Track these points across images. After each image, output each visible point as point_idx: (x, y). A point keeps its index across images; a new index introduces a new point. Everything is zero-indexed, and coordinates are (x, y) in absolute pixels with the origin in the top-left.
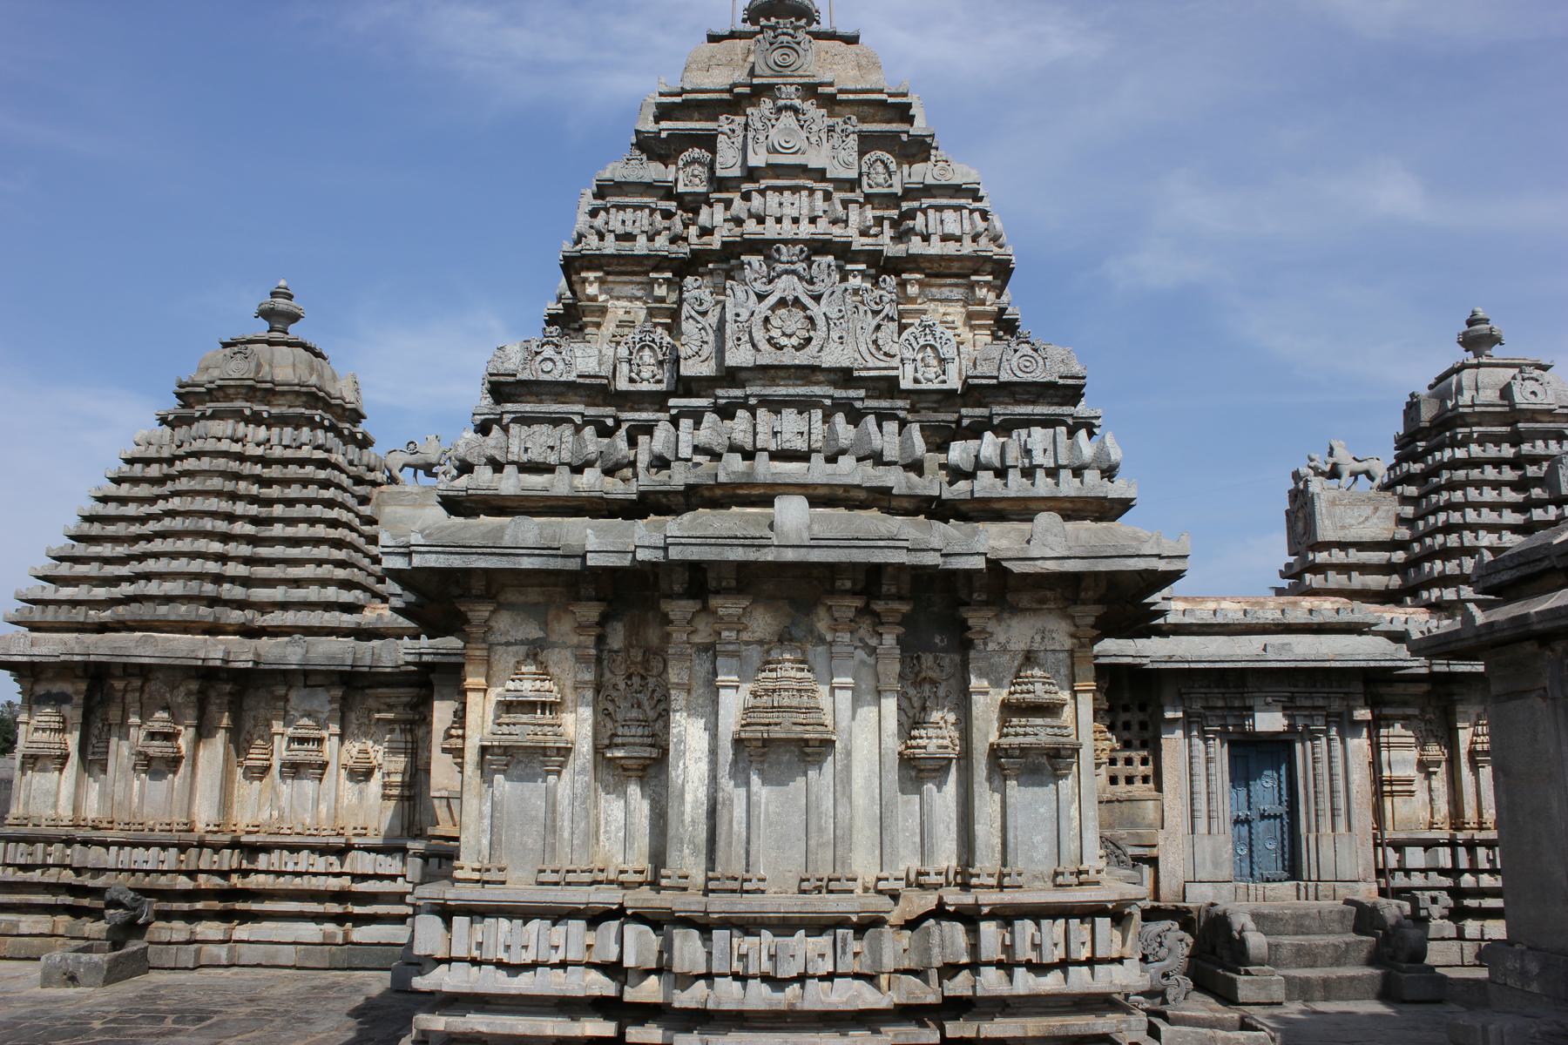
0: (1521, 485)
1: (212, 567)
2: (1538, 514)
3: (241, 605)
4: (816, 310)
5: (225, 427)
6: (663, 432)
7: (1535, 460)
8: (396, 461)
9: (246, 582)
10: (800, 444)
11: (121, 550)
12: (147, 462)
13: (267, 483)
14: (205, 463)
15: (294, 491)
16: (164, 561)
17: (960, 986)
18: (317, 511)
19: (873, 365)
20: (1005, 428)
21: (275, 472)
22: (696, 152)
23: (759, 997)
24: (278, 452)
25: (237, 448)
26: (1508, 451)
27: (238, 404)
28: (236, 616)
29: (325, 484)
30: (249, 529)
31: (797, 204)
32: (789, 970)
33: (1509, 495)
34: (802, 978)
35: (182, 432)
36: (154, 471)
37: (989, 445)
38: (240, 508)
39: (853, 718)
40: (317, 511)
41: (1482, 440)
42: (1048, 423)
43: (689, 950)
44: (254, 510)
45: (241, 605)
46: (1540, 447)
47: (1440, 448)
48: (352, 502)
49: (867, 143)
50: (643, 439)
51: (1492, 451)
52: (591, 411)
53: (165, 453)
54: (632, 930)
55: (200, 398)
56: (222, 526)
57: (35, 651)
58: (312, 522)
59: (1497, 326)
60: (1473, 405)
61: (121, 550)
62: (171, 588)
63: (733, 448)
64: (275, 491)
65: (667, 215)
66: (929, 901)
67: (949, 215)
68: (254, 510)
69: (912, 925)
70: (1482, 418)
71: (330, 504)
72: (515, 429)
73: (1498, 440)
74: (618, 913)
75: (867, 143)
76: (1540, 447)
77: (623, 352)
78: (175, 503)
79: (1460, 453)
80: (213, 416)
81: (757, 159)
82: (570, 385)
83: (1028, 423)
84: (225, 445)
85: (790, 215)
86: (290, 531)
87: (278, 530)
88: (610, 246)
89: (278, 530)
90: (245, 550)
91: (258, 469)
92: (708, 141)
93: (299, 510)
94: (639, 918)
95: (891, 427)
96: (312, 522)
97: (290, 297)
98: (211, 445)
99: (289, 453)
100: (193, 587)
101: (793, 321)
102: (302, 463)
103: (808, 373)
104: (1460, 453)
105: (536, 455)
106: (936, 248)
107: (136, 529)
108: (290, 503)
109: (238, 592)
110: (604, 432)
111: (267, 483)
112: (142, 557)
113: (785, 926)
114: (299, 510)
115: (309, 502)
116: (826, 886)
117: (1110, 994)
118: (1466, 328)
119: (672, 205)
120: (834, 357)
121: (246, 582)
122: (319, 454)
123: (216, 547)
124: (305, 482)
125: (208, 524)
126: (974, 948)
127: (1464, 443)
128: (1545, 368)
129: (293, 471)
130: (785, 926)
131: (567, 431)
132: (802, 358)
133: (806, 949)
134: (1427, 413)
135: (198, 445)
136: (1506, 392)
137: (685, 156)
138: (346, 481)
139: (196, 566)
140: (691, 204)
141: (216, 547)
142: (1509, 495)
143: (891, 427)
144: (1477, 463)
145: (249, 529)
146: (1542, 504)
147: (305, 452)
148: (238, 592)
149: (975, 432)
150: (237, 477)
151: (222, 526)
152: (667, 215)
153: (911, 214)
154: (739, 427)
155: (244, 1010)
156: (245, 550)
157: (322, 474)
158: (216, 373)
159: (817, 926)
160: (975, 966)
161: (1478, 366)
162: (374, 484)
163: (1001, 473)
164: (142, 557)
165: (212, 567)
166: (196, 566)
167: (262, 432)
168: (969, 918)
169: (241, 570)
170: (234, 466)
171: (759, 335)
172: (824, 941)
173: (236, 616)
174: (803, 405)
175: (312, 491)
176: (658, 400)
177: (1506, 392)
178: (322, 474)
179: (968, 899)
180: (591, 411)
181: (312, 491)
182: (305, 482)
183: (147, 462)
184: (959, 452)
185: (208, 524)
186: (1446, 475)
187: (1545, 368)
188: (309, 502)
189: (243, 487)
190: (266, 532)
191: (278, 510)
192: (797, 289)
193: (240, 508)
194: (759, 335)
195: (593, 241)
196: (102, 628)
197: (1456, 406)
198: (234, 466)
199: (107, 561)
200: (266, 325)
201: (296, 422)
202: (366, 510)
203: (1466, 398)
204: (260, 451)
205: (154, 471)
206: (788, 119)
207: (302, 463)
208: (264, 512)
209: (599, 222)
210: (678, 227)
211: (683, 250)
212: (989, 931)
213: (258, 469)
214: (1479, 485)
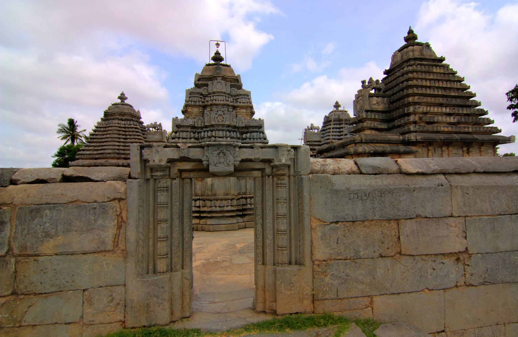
1: (117, 147)
3: (123, 154)
4: (224, 116)
5: (117, 121)
6: (203, 133)
9: (123, 150)
10: (222, 136)
11: (98, 144)
12: (101, 128)
13: (125, 132)
14: (113, 128)
15: (131, 133)
17: (245, 207)
18: (136, 137)
19: (233, 124)
20: (251, 132)
21: (127, 130)
22: (205, 87)
23: (218, 209)
24: (127, 126)
25: (119, 125)
27: (118, 117)
28: (123, 156)
29: (137, 132)
30: (123, 140)
31: (221, 98)
32: (222, 205)
34: (224, 206)
35: (107, 122)
36: (102, 129)
37: (248, 135)
38: (121, 136)
40: (136, 137)
42: (257, 132)
43: (208, 203)
44: (124, 137)
45: (123, 154)
48: (141, 135)
49: (232, 86)
50: (200, 134)
52: (192, 130)
53: (104, 126)
54: (201, 201)
55: (109, 115)
56: (118, 140)
58: (135, 139)
61: (98, 144)
62: (109, 151)
63: (213, 136)
64: (127, 133)
65: (201, 98)
66: (241, 196)
67: (244, 99)
68: (124, 137)
69: (238, 199)
71: (138, 135)
72: (181, 133)
74: (199, 199)
75: (232, 86)
77: (196, 120)
78: (108, 136)
80: (113, 119)
81: (215, 90)
82: (188, 126)
83: (254, 132)
84: (117, 125)
85: (220, 100)
86: (131, 141)
87: (129, 140)
88: (193, 103)
89: (129, 140)
90: (123, 144)
91: (124, 129)
92: (207, 85)
93: (132, 137)
94: (202, 200)
95: (235, 133)
96: (135, 139)
98: (114, 125)
99: (129, 126)
100: (114, 151)
101: (221, 118)
102: (132, 128)
103: (223, 125)
105: (184, 136)
106: (242, 104)
107: (100, 140)
108: (130, 135)
109: (123, 152)
110: (194, 133)
111: (125, 132)
112: (102, 146)
113: (222, 200)
114: (132, 137)
115: (134, 135)
116: (227, 195)
117: (63, 146)
119: (202, 96)
120: (227, 123)
121: (123, 150)
122: (135, 126)
123: (117, 144)
124: (133, 132)
125: (116, 140)
126: (246, 202)
129: (130, 129)
130: (222, 200)
131: (189, 133)
132: (222, 123)
133: (225, 203)
135: (111, 125)
137: (204, 88)
138: (140, 131)
139: (114, 147)
140: (205, 96)
141: (117, 144)
143: (235, 133)
145: (123, 140)
147: (132, 126)
148: (123, 152)
149: (247, 133)
150: (119, 131)
151: (118, 140)
152: (201, 98)
153: (238, 99)
154: (214, 133)
155: (424, 145)
156: (123, 144)
157: (136, 130)
158: (112, 111)
159: (226, 200)
160: (247, 204)
162: (145, 131)
163: (250, 139)
164: (102, 146)
165: (117, 147)
166: (114, 147)
167: (123, 122)
168: (246, 198)
169: (123, 148)
170: (119, 129)
171: (216, 120)
172: (226, 202)
173: (123, 156)
174: (223, 130)
175: (135, 133)
176: (202, 128)
178: (136, 130)
179: (246, 196)
180: (192, 130)
181: (135, 133)
182: (133, 132)
183: (101, 128)
184: (244, 136)
185: (116, 140)
188: (134, 135)
189: (121, 132)
190: (126, 141)
191: (128, 137)
192: (221, 113)
193: (121, 136)
194: (216, 120)
195: (190, 102)
196: (96, 159)
198: (119, 129)
199: (95, 146)
201: (130, 120)
202: (144, 136)
204: (124, 126)
205: (102, 129)
206: (219, 84)
207: (132, 128)
208: (126, 137)
209: (191, 99)
210: (203, 100)
211: (204, 104)
212: (248, 200)
213: (124, 129)
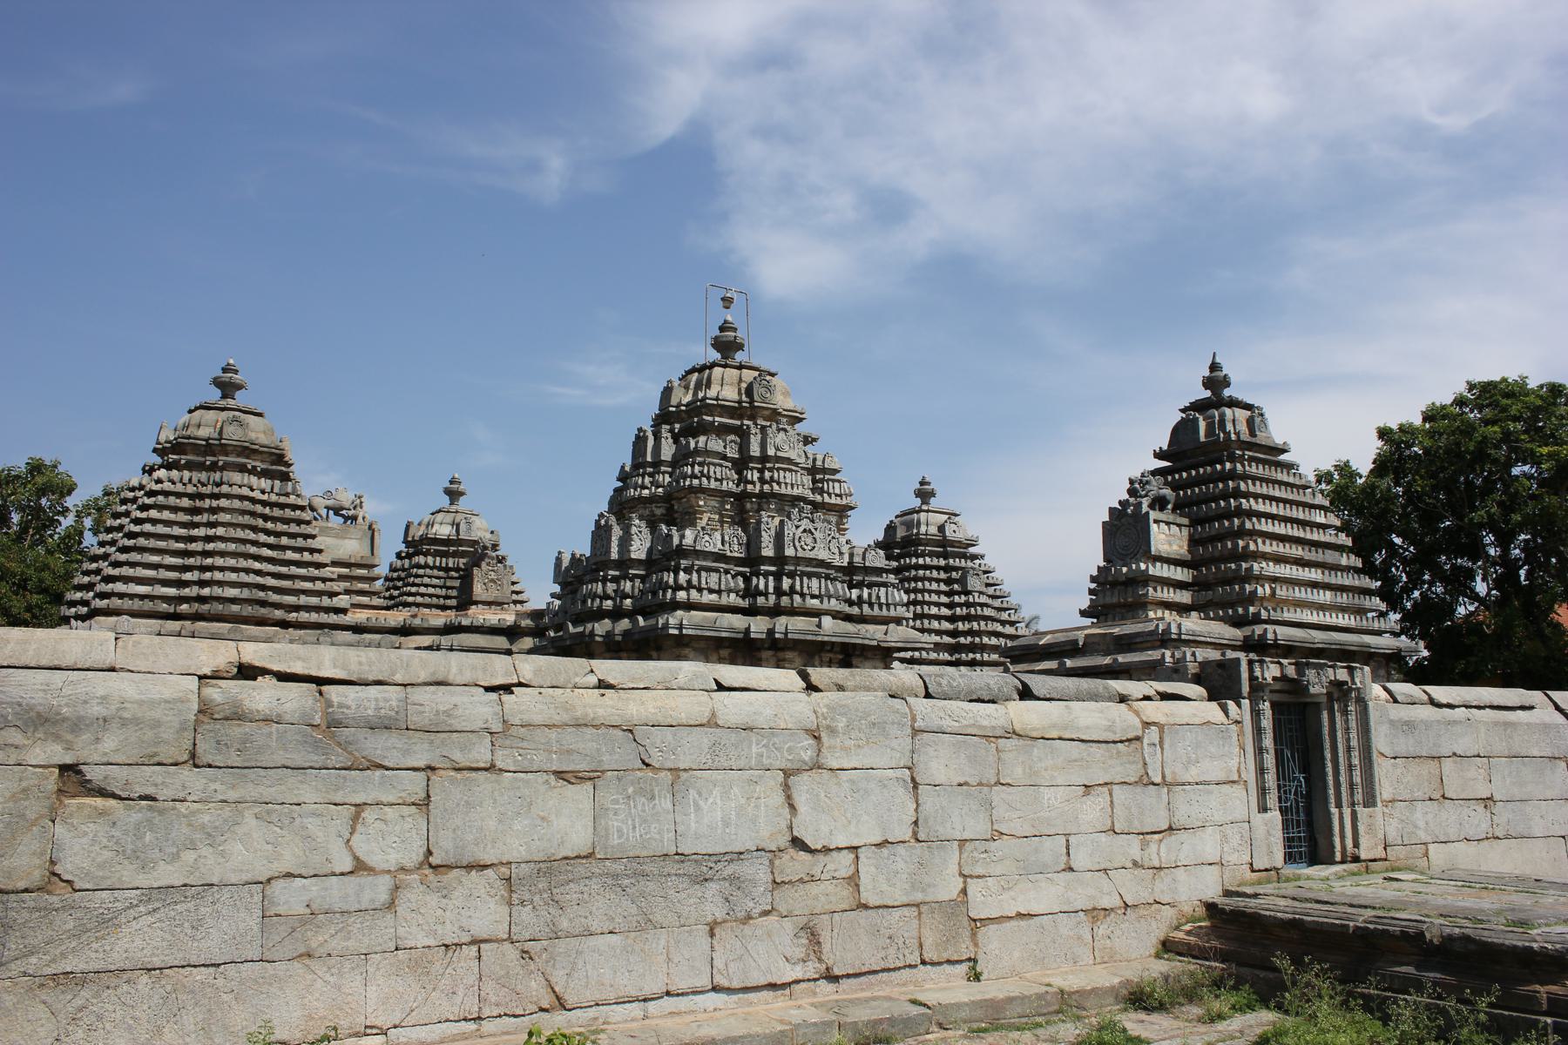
0: (948, 582)
2: (957, 598)
7: (956, 569)
8: (320, 503)
16: (139, 569)
26: (942, 562)
33: (943, 587)
39: (488, 689)
41: (931, 554)
46: (957, 562)
47: (910, 556)
51: (935, 562)
57: (1121, 719)
59: (741, 334)
60: (717, 399)
70: (928, 543)
73: (938, 555)
76: (957, 562)
79: (921, 561)
97: (236, 372)
99: (283, 500)
104: (921, 561)
118: (717, 333)
127: (923, 555)
128: (773, 375)
134: (901, 533)
136: (941, 528)
142: (943, 587)
144: (925, 567)
146: (959, 593)
161: (725, 366)
177: (941, 528)
186: (913, 573)
187: (773, 375)
197: (705, 398)
200: (218, 393)
203: (712, 393)
206: (782, 434)
214: (930, 580)
